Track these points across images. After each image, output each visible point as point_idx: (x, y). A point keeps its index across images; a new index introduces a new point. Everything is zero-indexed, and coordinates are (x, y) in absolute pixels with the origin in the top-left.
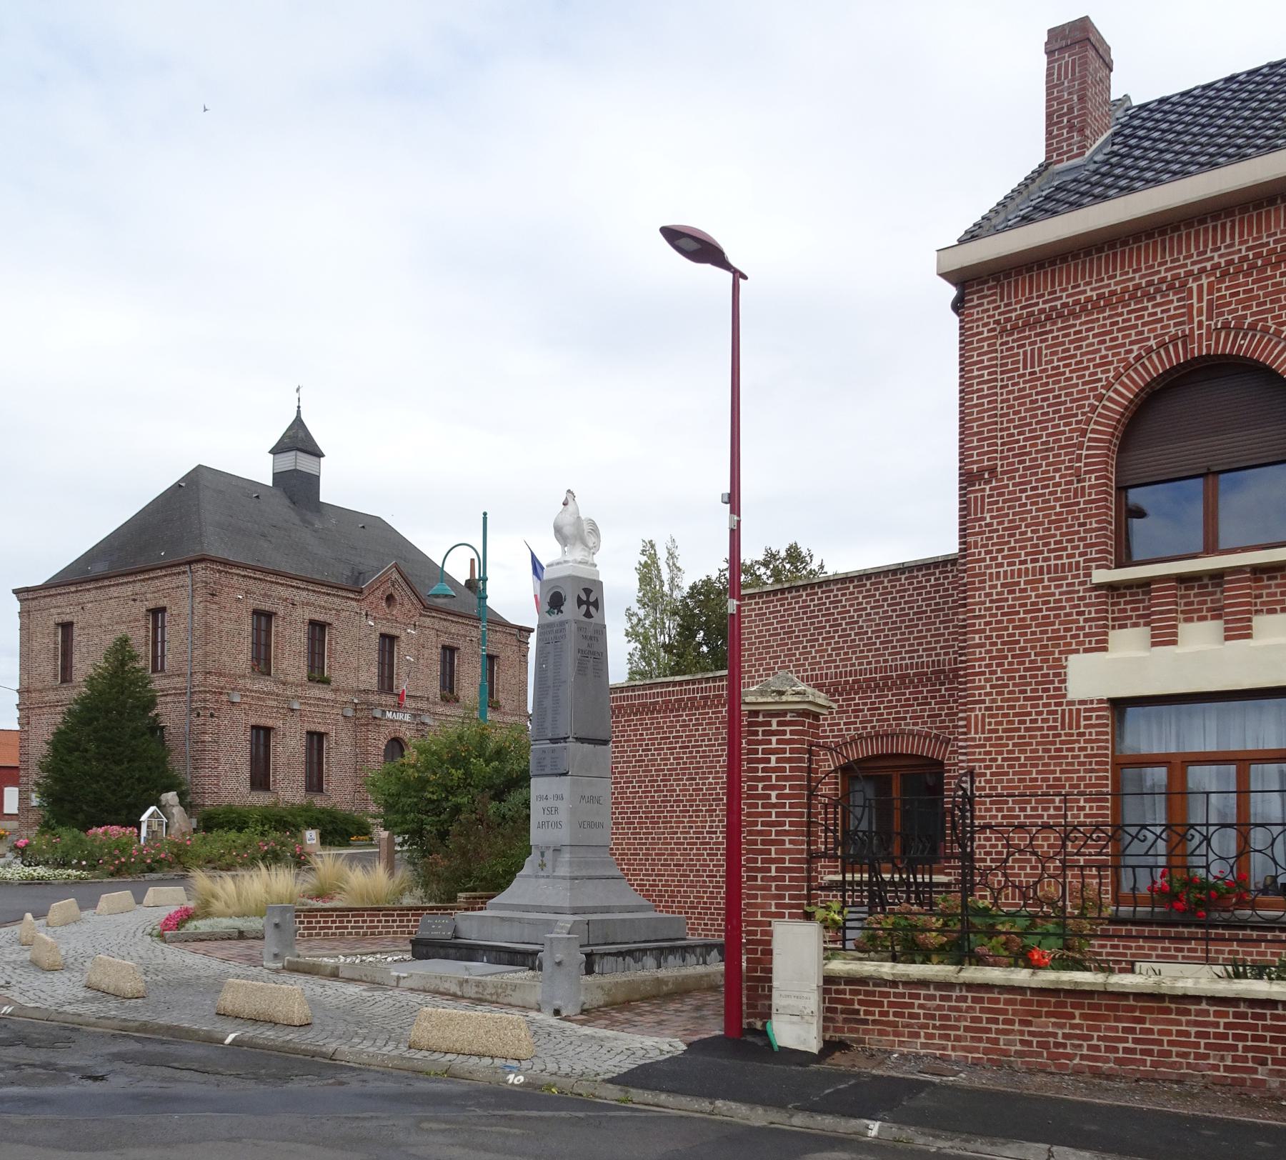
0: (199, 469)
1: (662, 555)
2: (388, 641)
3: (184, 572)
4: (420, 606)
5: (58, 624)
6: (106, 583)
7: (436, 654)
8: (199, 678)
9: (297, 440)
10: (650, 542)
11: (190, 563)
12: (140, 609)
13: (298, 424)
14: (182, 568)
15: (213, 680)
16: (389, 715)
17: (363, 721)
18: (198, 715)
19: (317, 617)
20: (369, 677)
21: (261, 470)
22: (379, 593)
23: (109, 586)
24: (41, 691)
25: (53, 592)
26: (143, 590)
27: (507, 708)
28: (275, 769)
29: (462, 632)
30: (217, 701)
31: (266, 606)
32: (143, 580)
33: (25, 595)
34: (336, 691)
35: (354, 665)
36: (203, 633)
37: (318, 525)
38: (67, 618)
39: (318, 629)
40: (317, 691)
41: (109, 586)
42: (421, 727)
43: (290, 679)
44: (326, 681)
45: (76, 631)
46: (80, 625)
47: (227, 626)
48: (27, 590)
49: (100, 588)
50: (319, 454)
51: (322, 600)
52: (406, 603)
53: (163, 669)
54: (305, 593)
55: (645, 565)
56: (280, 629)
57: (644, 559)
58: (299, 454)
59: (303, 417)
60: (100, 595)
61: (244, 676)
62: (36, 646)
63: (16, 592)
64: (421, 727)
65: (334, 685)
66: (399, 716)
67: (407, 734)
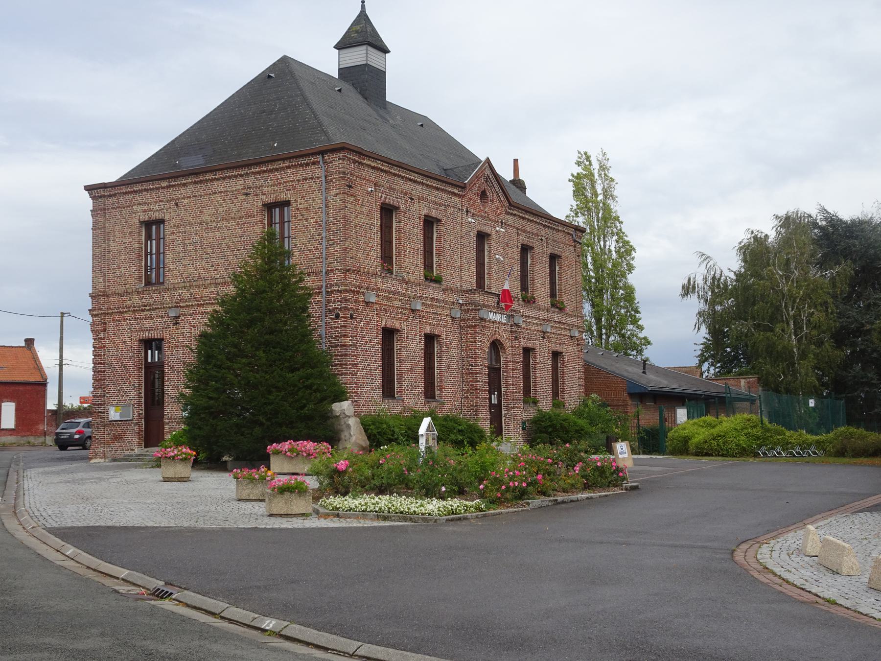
0: (285, 61)
1: (596, 166)
3: (314, 163)
4: (506, 204)
5: (141, 223)
6: (209, 176)
7: (515, 253)
8: (336, 277)
9: (362, 35)
10: (586, 153)
11: (323, 153)
12: (255, 204)
13: (363, 18)
15: (351, 278)
17: (469, 323)
18: (337, 316)
20: (469, 279)
21: (328, 63)
22: (475, 190)
23: (212, 180)
24: (121, 295)
25: (138, 187)
26: (258, 183)
28: (401, 375)
29: (535, 231)
30: (356, 301)
31: (391, 200)
32: (259, 173)
33: (102, 192)
34: (445, 290)
36: (327, 226)
39: (429, 223)
40: (431, 292)
41: (212, 180)
42: (514, 329)
43: (411, 277)
44: (438, 281)
46: (173, 222)
48: (104, 186)
49: (201, 182)
50: (385, 51)
51: (434, 195)
55: (578, 177)
56: (402, 225)
57: (579, 170)
58: (370, 48)
59: (368, 12)
60: (200, 189)
61: (376, 274)
62: (114, 246)
63: (89, 188)
64: (514, 329)
67: (504, 336)
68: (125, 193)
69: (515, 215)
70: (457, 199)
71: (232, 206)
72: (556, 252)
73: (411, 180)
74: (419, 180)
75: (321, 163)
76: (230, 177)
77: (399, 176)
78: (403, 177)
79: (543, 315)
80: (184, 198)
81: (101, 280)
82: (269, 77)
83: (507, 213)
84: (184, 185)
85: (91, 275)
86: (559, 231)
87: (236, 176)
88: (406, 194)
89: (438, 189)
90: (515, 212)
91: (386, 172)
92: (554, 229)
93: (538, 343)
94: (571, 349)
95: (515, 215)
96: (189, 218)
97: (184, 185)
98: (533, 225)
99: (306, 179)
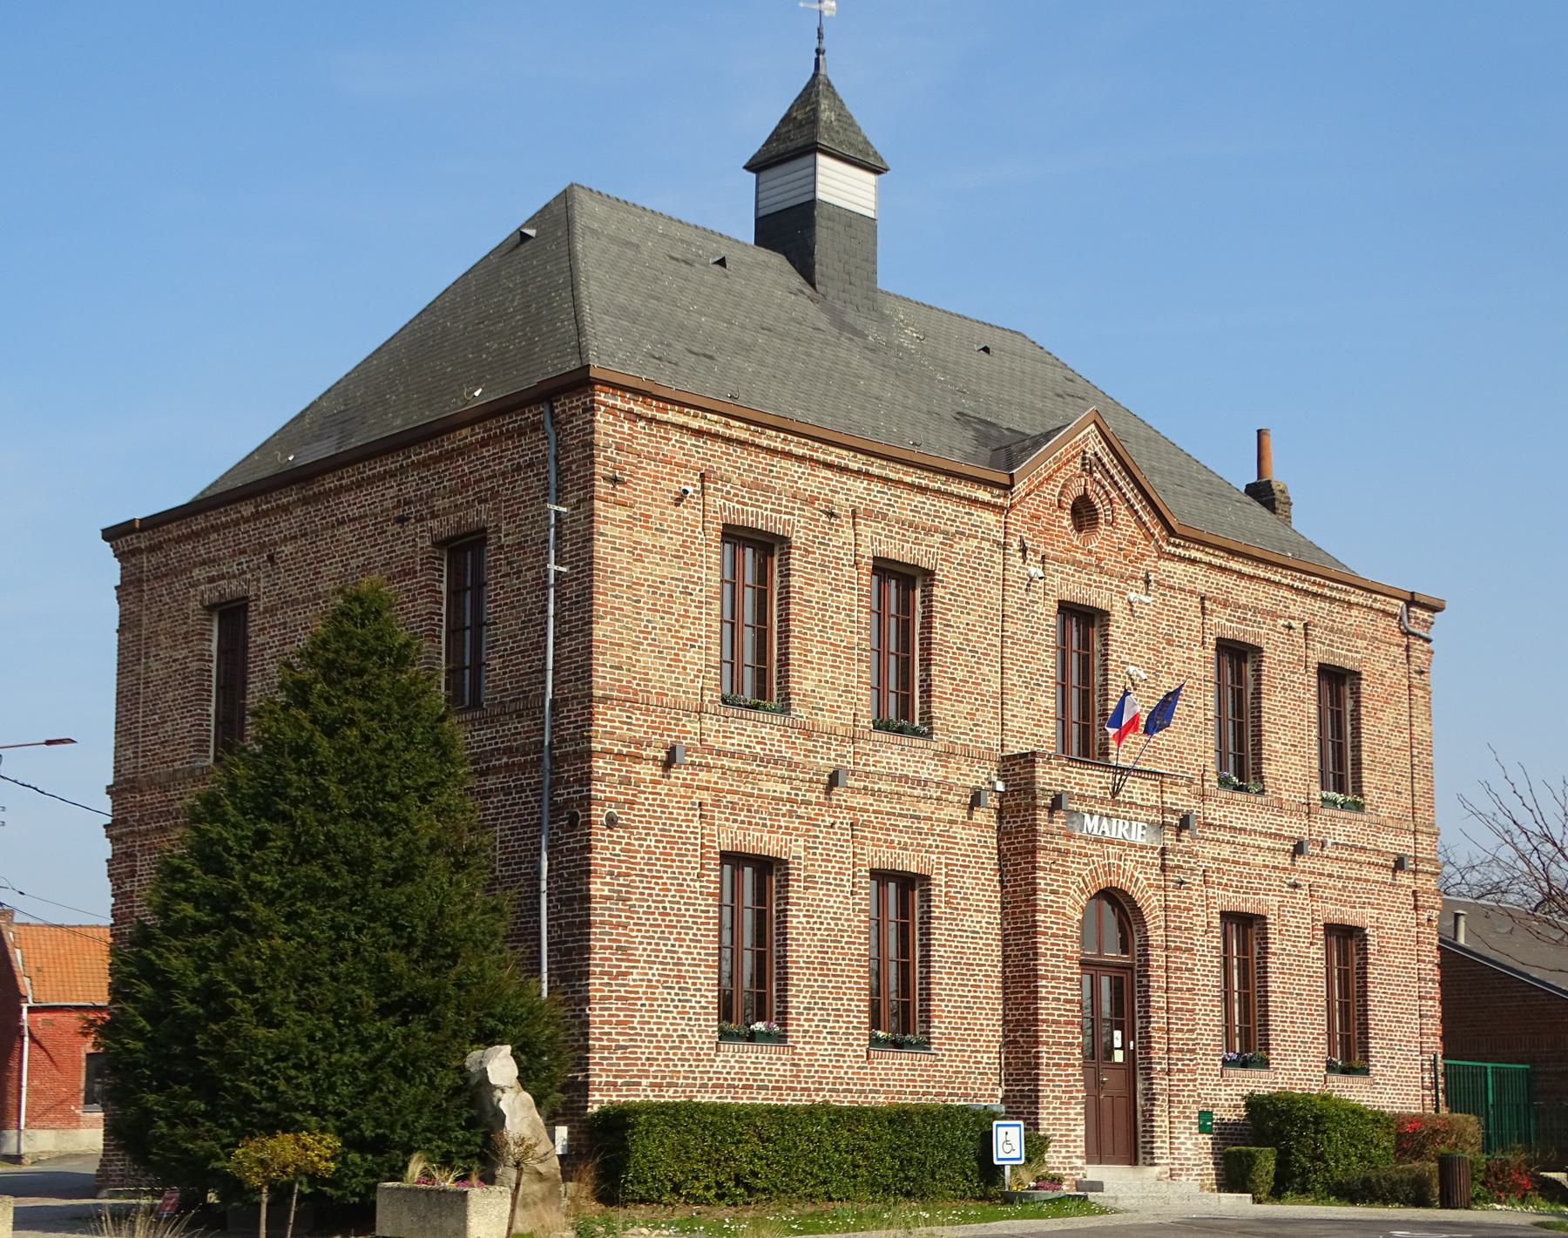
2: (1082, 621)
3: (536, 427)
12: (420, 539)
14: (529, 415)
16: (1091, 823)
19: (892, 551)
27: (1384, 812)
29: (1266, 604)
30: (625, 781)
31: (759, 516)
32: (424, 464)
35: (996, 691)
37: (532, 1142)
38: (232, 588)
39: (901, 581)
41: (338, 491)
43: (825, 720)
45: (255, 620)
47: (655, 569)
52: (1122, 526)
53: (476, 704)
54: (860, 485)
59: (829, 70)
63: (110, 534)
65: (940, 740)
66: (1116, 829)
68: (179, 540)
69: (1193, 561)
70: (990, 517)
71: (373, 552)
72: (1338, 662)
73: (828, 466)
74: (854, 466)
75: (548, 425)
76: (370, 481)
77: (788, 455)
78: (801, 459)
79: (1295, 826)
80: (285, 540)
81: (129, 754)
82: (525, 237)
83: (1162, 554)
84: (285, 509)
85: (112, 743)
86: (1350, 605)
87: (382, 477)
88: (811, 501)
89: (923, 490)
90: (1194, 554)
91: (742, 443)
92: (1332, 600)
93: (1273, 901)
94: (1393, 919)
95: (1193, 561)
96: (294, 591)
97: (285, 509)
98: (1260, 590)
99: (518, 468)
